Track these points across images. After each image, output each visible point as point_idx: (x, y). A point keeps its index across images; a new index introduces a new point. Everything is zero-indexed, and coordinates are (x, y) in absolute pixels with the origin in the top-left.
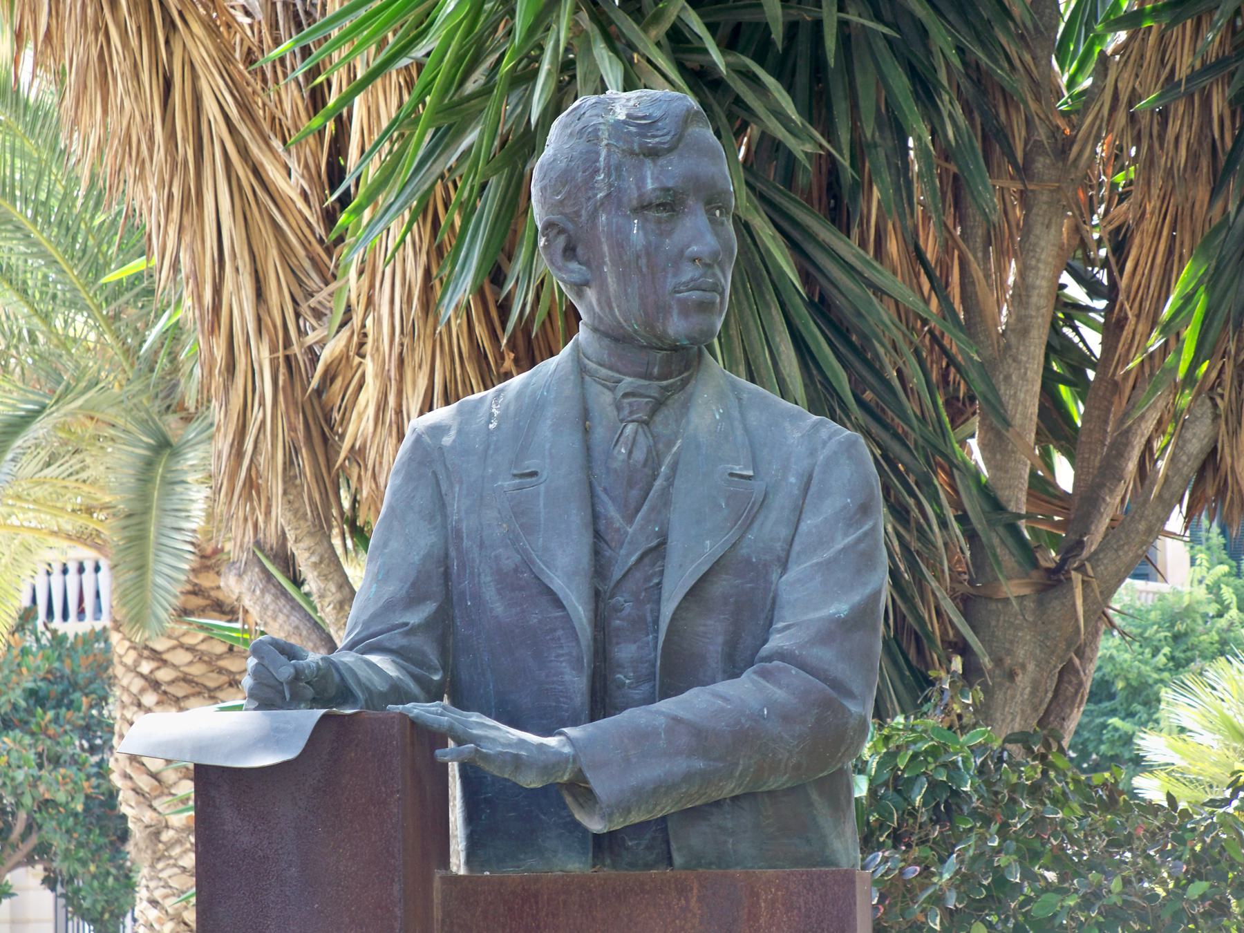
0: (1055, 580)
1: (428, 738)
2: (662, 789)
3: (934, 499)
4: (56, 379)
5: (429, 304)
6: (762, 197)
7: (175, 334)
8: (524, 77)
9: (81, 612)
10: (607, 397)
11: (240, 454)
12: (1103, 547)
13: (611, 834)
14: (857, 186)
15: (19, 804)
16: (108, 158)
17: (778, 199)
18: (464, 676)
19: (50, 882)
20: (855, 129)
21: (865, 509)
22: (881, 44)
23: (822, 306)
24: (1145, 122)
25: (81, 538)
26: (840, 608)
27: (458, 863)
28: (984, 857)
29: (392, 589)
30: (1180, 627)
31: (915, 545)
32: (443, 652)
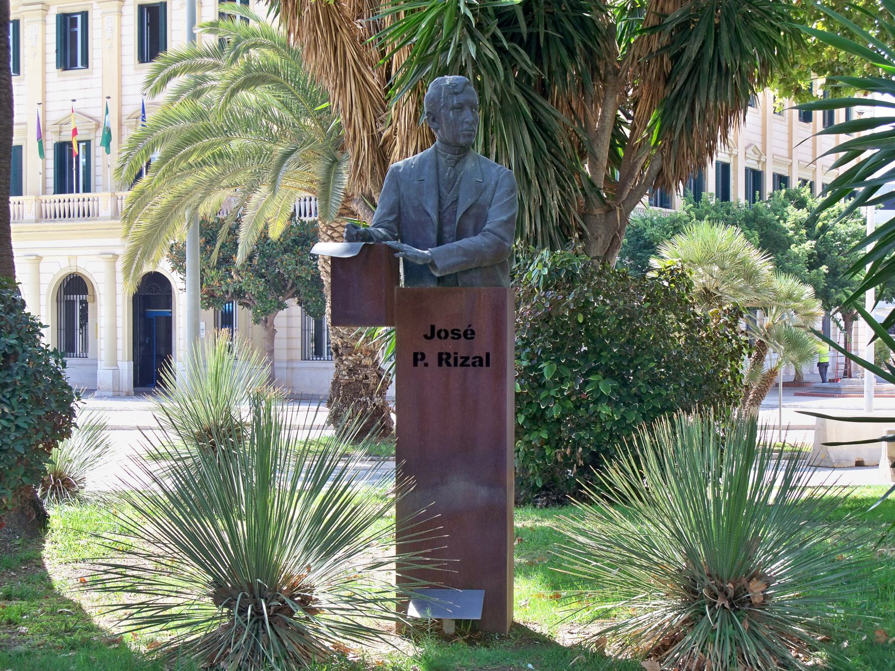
0: (610, 210)
1: (393, 250)
2: (454, 265)
3: (573, 183)
4: (301, 138)
5: (416, 119)
6: (520, 87)
7: (339, 126)
8: (446, 49)
9: (311, 214)
10: (443, 159)
11: (357, 166)
12: (627, 198)
13: (443, 277)
14: (549, 85)
15: (289, 277)
16: (317, 71)
17: (525, 88)
18: (404, 234)
19: (300, 303)
20: (549, 67)
21: (512, 191)
22: (558, 41)
23: (539, 123)
24: (642, 65)
25: (309, 190)
26: (504, 218)
27: (402, 284)
28: (582, 293)
29: (385, 210)
30: (676, 225)
31: (567, 197)
32: (399, 228)
